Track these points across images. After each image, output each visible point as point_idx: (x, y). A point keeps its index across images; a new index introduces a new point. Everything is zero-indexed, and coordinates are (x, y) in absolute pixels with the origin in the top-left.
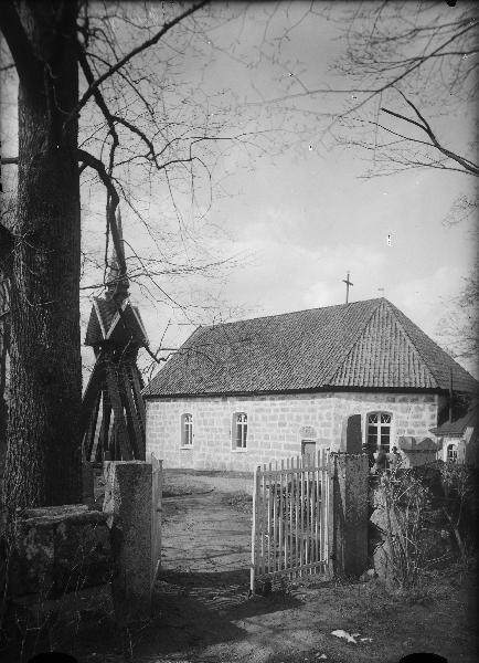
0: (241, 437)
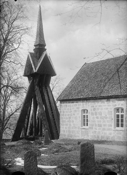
0: (85, 121)
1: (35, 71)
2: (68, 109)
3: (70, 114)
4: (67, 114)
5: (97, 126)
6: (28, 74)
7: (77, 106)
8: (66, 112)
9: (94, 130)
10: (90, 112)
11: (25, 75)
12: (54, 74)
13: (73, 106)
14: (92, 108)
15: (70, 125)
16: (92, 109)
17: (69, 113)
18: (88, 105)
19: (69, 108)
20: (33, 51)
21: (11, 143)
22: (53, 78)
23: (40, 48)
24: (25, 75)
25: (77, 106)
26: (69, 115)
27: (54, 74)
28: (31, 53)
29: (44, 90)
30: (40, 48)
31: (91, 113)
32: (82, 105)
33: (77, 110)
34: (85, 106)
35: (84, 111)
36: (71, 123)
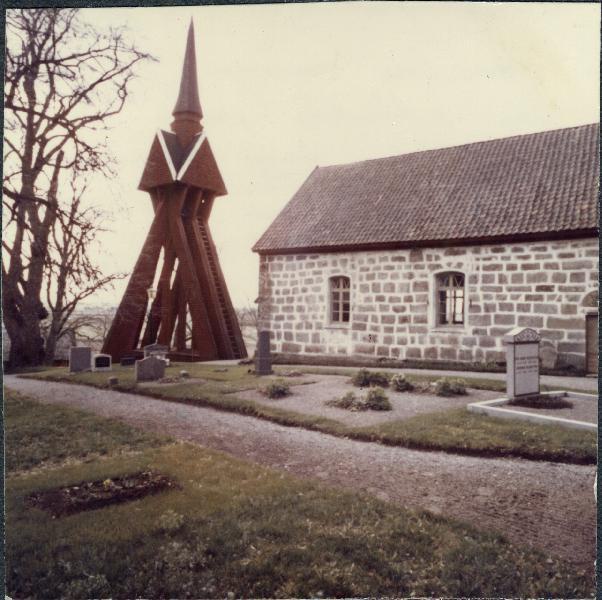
0: (341, 311)
1: (177, 176)
2: (286, 276)
3: (291, 288)
4: (281, 289)
5: (391, 325)
6: (154, 183)
7: (316, 268)
8: (279, 283)
9: (368, 332)
10: (358, 284)
11: (143, 187)
12: (220, 190)
13: (301, 267)
14: (364, 274)
15: (291, 318)
16: (364, 277)
17: (288, 287)
18: (353, 267)
19: (290, 273)
20: (168, 129)
21: (53, 392)
22: (218, 203)
23: (188, 114)
24: (143, 187)
25: (316, 268)
26: (286, 292)
27: (220, 190)
28: (165, 134)
29: (195, 223)
30: (188, 114)
31: (362, 286)
32: (330, 266)
33: (314, 277)
34: (339, 267)
35: (335, 281)
36: (296, 314)
